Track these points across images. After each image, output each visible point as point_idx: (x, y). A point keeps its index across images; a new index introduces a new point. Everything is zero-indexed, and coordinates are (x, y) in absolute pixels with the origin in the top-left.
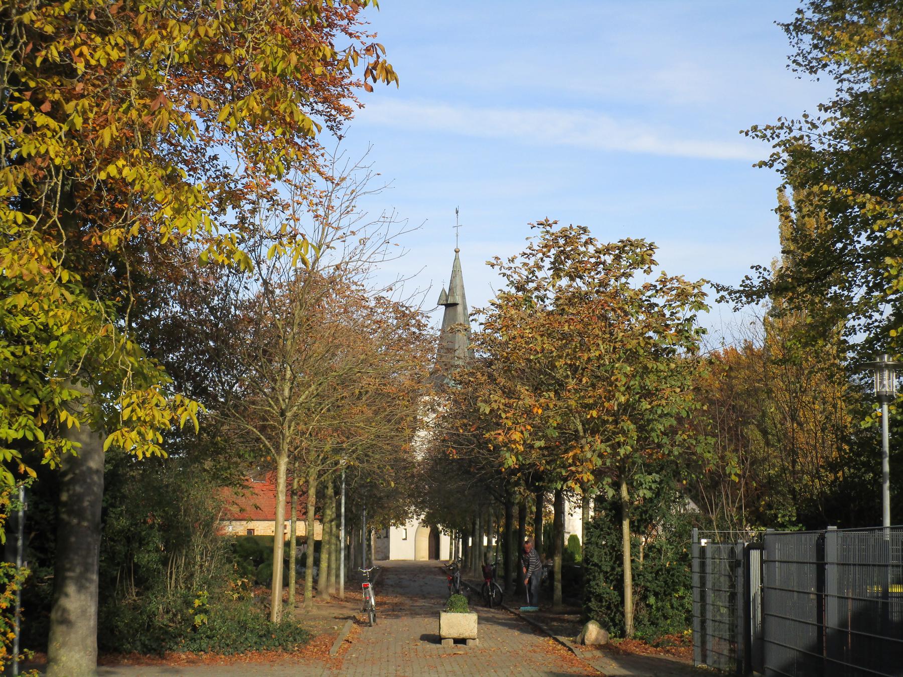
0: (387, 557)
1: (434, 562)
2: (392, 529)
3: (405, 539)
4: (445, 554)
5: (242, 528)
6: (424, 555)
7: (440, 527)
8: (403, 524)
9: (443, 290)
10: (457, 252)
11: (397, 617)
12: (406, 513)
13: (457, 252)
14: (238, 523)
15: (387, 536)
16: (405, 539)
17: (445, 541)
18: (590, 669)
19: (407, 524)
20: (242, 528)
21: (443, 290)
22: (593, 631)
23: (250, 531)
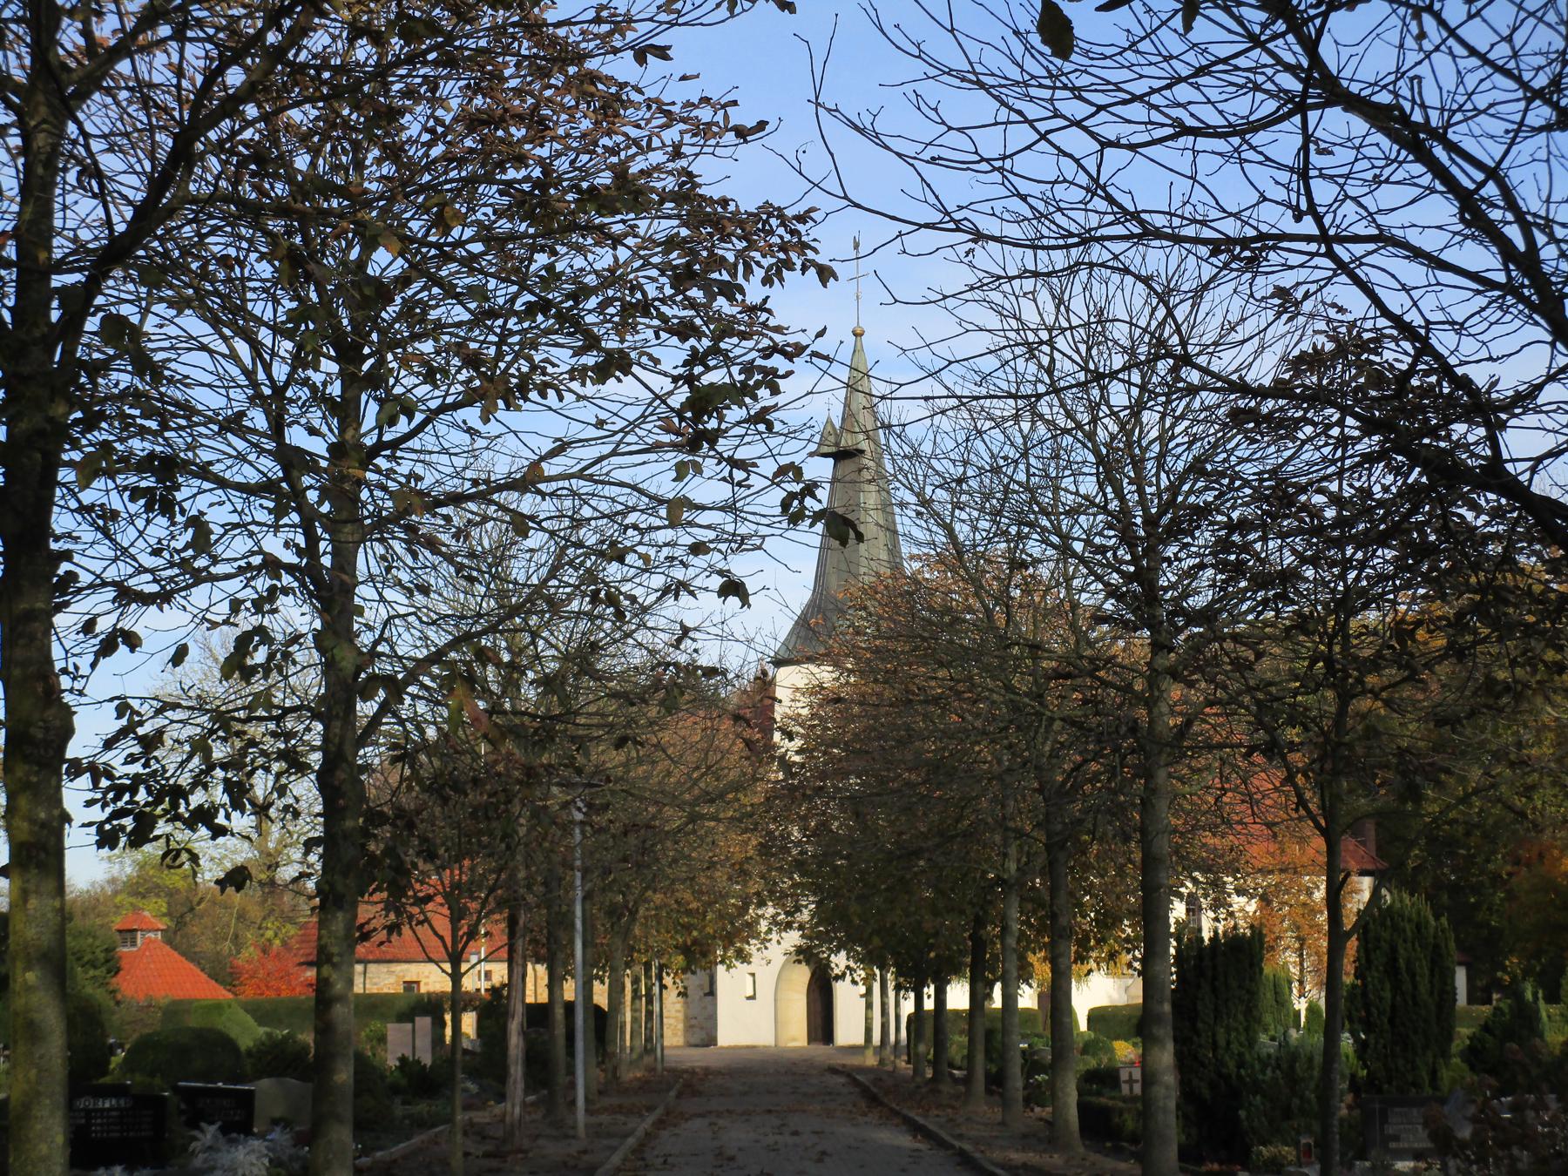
0: (711, 1040)
1: (820, 1050)
2: (721, 969)
3: (753, 998)
4: (849, 1027)
5: (392, 980)
6: (797, 1034)
7: (840, 961)
8: (743, 957)
9: (829, 421)
10: (858, 334)
11: (174, 1003)
12: (751, 926)
13: (858, 334)
14: (383, 968)
15: (711, 993)
16: (753, 998)
17: (848, 1000)
18: (272, 995)
19: (756, 957)
20: (392, 980)
21: (829, 421)
22: (363, 777)
23: (410, 985)
